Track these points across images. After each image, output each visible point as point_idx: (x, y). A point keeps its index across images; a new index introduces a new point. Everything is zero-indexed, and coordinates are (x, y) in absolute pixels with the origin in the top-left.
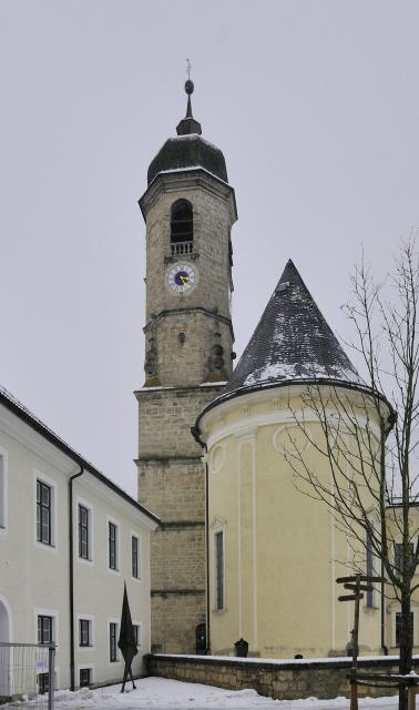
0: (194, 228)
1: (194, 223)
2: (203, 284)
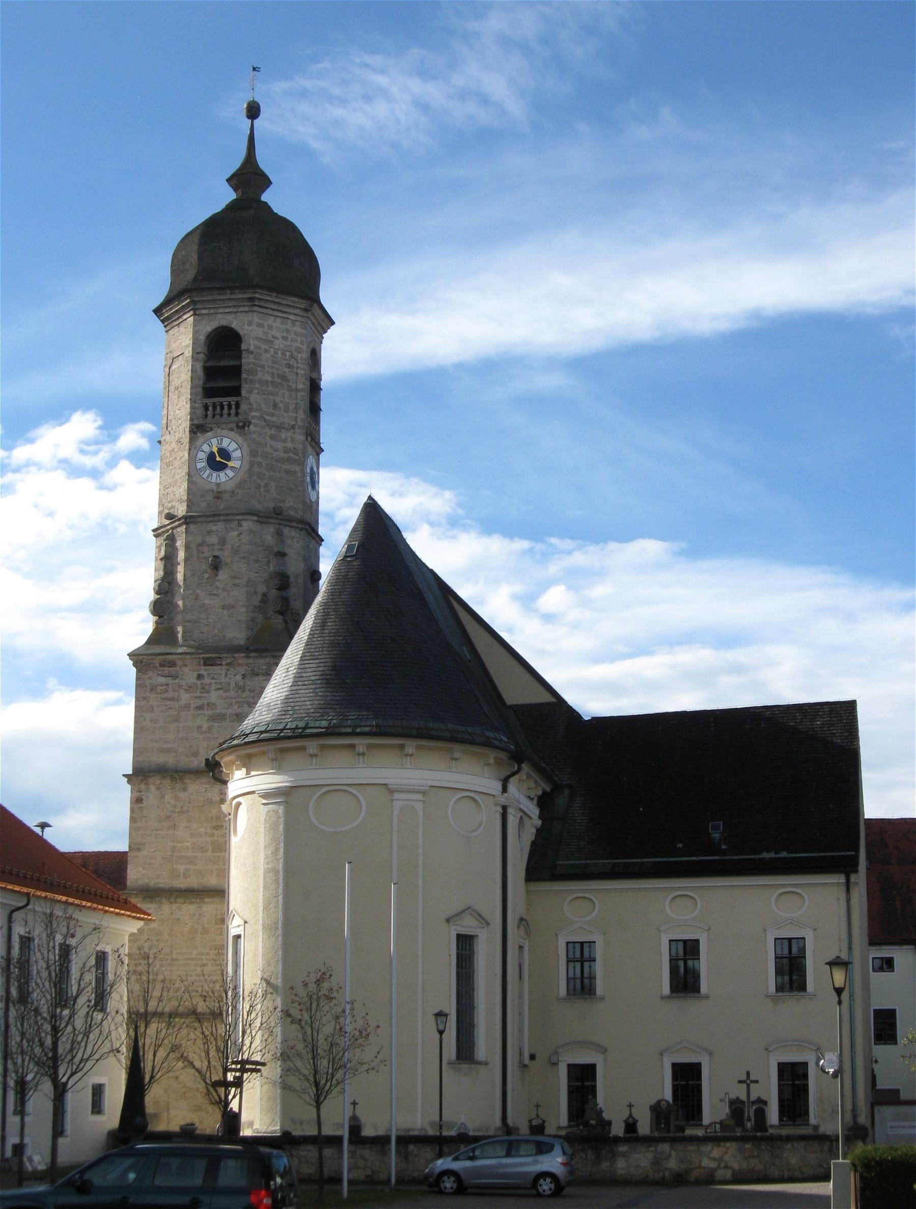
0: (244, 376)
2: (256, 469)
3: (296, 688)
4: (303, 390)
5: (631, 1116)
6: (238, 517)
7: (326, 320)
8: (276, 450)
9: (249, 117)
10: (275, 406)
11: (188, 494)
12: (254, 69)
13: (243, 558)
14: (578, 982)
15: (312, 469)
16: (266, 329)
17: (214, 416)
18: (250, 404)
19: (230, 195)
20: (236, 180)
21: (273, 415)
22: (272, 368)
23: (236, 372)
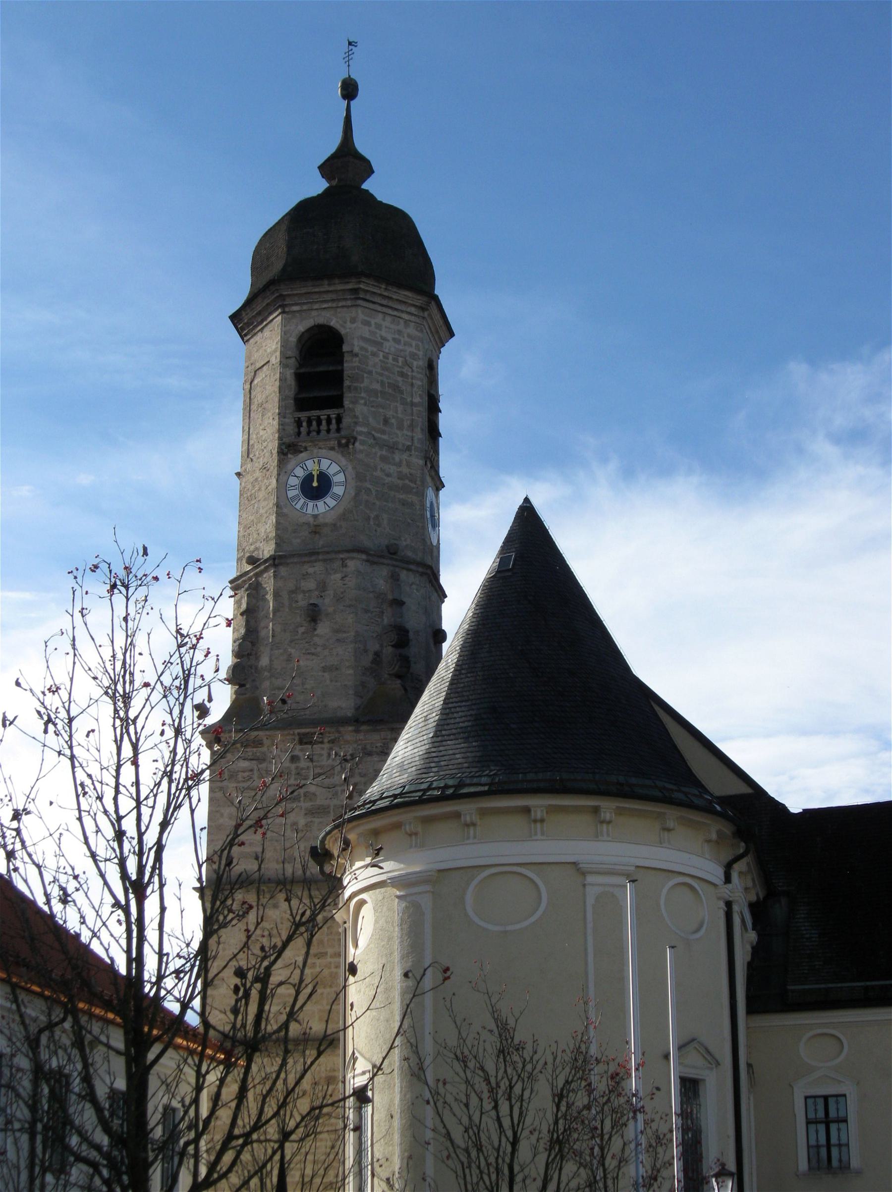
0: (347, 383)
1: (346, 373)
3: (440, 739)
6: (342, 556)
7: (444, 328)
8: (388, 475)
10: (386, 421)
11: (277, 529)
12: (350, 43)
13: (350, 606)
14: (823, 1151)
15: (432, 504)
16: (373, 328)
17: (309, 433)
18: (356, 417)
20: (326, 169)
21: (384, 432)
22: (381, 375)
23: (337, 379)
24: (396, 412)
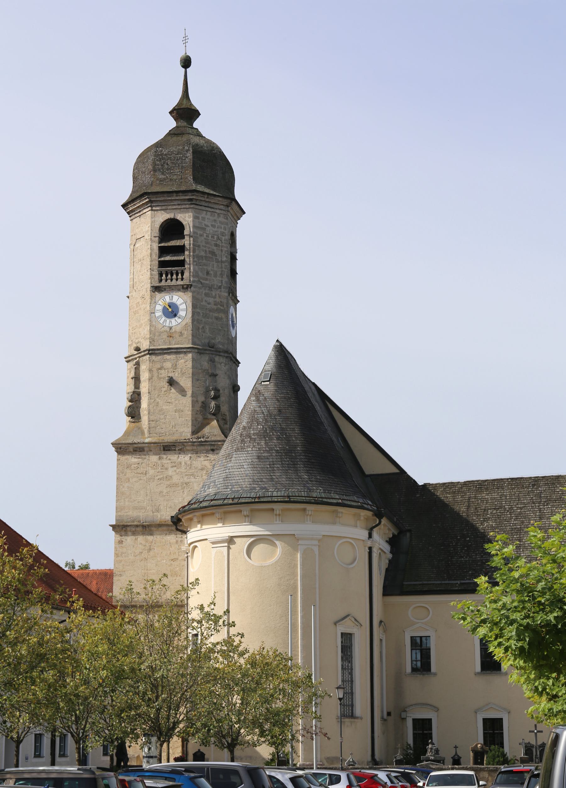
4: (226, 261)
5: (456, 754)
8: (209, 304)
9: (183, 67)
10: (208, 273)
15: (232, 315)
19: (172, 124)
21: (206, 280)
22: (205, 247)
24: (213, 267)
